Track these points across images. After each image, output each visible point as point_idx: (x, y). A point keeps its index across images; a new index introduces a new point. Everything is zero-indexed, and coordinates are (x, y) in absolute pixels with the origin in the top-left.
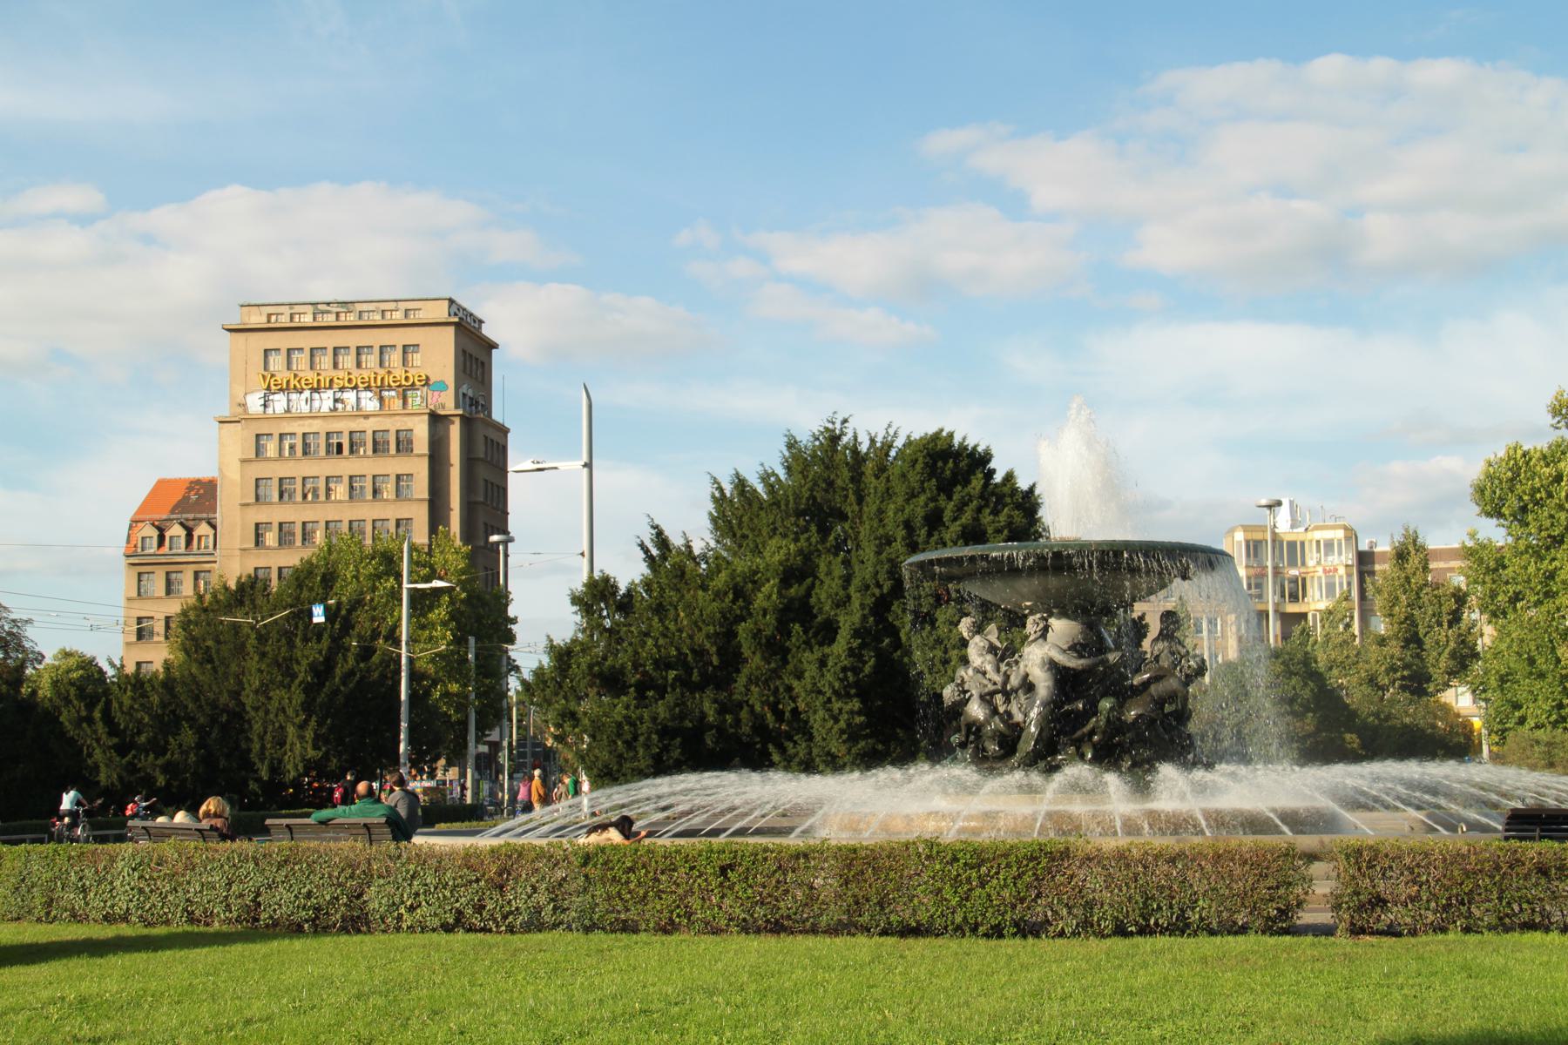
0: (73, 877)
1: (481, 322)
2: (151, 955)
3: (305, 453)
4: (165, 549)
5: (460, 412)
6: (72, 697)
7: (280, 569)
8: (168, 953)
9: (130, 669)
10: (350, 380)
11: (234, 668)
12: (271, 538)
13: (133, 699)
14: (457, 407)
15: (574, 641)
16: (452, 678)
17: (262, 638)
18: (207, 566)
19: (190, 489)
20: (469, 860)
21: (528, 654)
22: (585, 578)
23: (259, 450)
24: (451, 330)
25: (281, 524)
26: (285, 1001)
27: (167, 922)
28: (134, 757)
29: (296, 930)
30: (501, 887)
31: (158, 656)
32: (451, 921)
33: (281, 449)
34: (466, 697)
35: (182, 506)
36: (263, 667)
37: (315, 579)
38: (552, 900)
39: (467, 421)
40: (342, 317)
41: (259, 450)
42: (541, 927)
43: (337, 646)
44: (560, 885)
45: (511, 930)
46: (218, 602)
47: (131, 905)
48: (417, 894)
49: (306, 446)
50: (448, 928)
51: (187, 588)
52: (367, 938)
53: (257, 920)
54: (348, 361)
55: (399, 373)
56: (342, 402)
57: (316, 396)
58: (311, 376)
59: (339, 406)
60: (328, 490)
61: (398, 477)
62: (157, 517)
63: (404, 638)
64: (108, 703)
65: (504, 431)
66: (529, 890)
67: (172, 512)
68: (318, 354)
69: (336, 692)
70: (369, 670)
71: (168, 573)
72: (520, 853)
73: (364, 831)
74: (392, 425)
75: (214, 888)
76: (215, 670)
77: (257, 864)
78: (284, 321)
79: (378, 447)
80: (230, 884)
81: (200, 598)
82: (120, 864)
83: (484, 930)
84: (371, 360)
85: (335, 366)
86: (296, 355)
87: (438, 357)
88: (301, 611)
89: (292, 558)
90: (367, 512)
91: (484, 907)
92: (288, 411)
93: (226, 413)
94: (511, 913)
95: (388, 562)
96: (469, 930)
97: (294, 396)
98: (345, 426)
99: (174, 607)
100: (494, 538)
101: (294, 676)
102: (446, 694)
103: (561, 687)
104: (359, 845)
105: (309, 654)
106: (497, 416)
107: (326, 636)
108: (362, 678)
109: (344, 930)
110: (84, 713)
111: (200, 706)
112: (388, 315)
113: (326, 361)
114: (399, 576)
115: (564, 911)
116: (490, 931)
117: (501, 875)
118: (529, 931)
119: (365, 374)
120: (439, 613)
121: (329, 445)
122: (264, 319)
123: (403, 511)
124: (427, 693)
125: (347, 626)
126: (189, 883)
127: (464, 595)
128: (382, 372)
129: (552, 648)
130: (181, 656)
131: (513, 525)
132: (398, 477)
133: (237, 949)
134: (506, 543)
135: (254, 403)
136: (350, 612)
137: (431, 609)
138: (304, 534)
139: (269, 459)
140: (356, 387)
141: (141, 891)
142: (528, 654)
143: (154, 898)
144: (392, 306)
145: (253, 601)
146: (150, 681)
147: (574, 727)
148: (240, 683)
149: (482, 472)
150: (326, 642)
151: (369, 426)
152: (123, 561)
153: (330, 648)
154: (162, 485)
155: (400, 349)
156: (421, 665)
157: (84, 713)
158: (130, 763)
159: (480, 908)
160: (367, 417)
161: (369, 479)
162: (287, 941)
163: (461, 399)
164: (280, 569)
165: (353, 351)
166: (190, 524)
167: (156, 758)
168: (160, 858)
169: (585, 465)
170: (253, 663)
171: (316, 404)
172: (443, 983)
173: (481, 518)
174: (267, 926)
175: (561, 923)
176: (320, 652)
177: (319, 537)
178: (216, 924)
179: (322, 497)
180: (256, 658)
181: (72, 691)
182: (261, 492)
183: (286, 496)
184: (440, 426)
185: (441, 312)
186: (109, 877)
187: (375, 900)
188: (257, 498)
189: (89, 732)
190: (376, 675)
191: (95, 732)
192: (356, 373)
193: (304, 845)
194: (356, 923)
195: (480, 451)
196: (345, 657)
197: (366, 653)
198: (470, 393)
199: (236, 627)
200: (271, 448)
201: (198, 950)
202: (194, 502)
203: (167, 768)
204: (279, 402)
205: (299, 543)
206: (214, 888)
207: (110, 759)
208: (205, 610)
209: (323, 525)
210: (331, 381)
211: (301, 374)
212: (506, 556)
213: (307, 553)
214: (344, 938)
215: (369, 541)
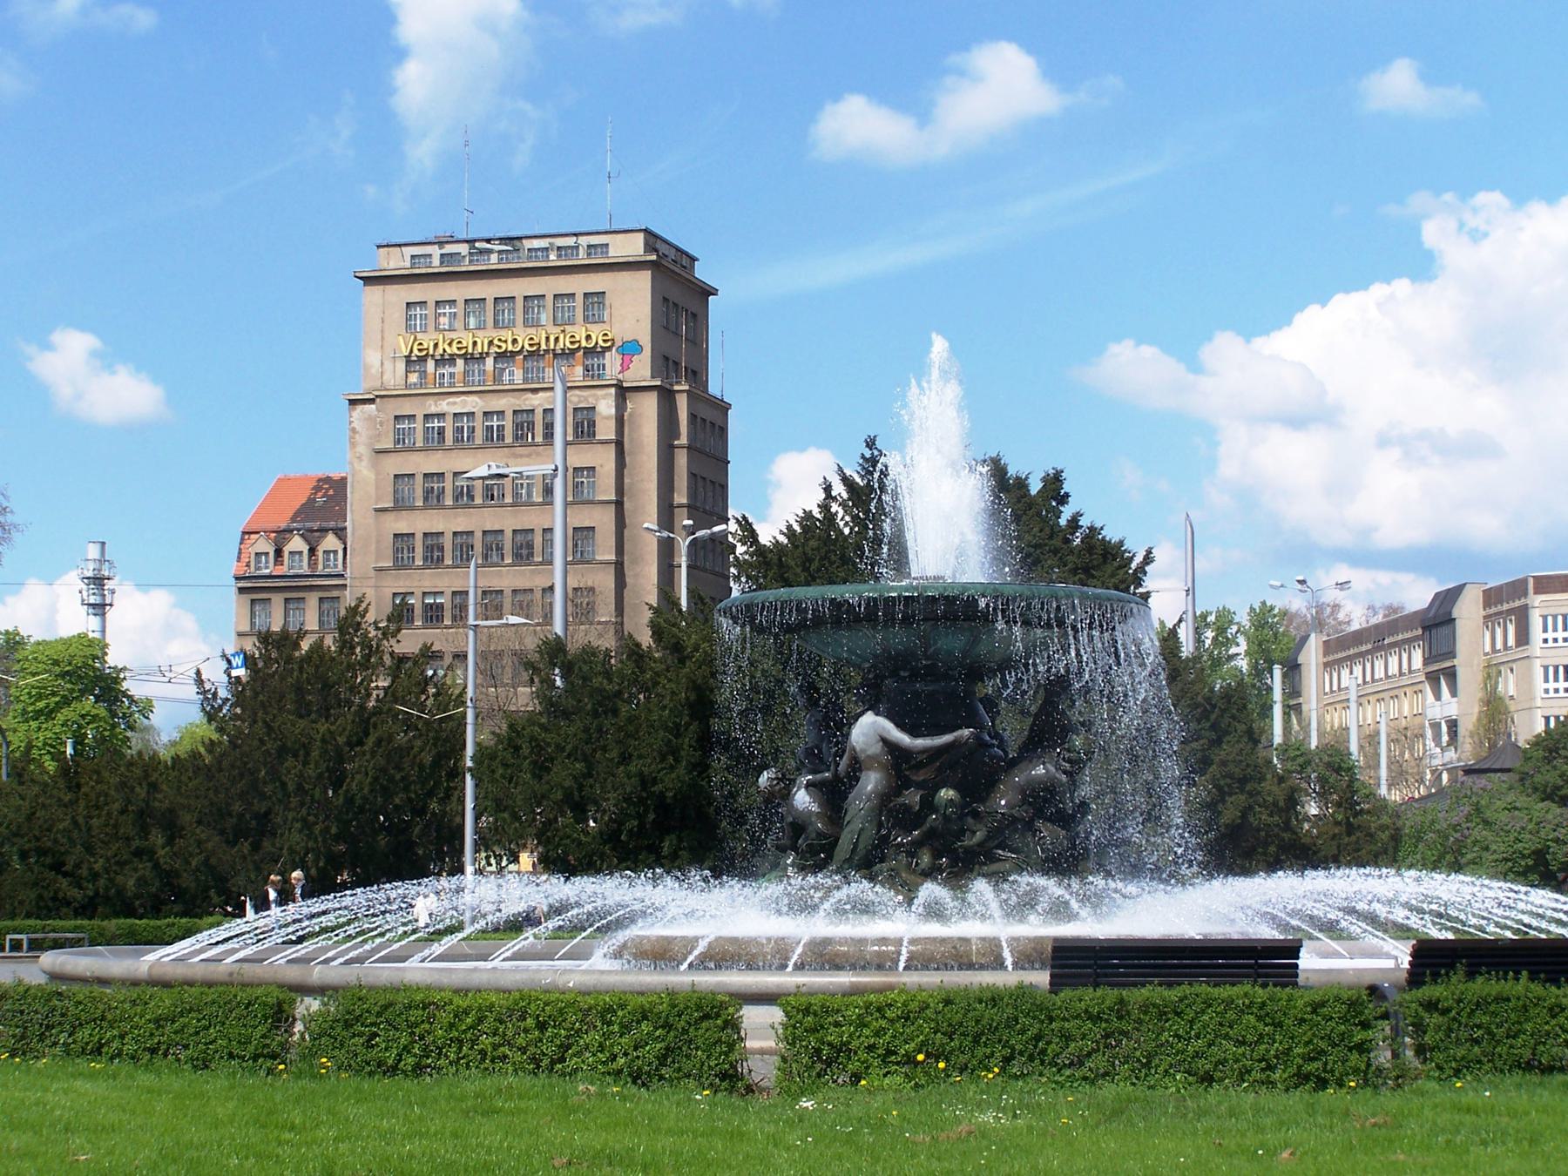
1: (694, 259)
14: (653, 377)
18: (335, 593)
19: (317, 489)
67: (293, 520)
87: (631, 307)
122: (408, 264)
144: (570, 241)
185: (633, 247)
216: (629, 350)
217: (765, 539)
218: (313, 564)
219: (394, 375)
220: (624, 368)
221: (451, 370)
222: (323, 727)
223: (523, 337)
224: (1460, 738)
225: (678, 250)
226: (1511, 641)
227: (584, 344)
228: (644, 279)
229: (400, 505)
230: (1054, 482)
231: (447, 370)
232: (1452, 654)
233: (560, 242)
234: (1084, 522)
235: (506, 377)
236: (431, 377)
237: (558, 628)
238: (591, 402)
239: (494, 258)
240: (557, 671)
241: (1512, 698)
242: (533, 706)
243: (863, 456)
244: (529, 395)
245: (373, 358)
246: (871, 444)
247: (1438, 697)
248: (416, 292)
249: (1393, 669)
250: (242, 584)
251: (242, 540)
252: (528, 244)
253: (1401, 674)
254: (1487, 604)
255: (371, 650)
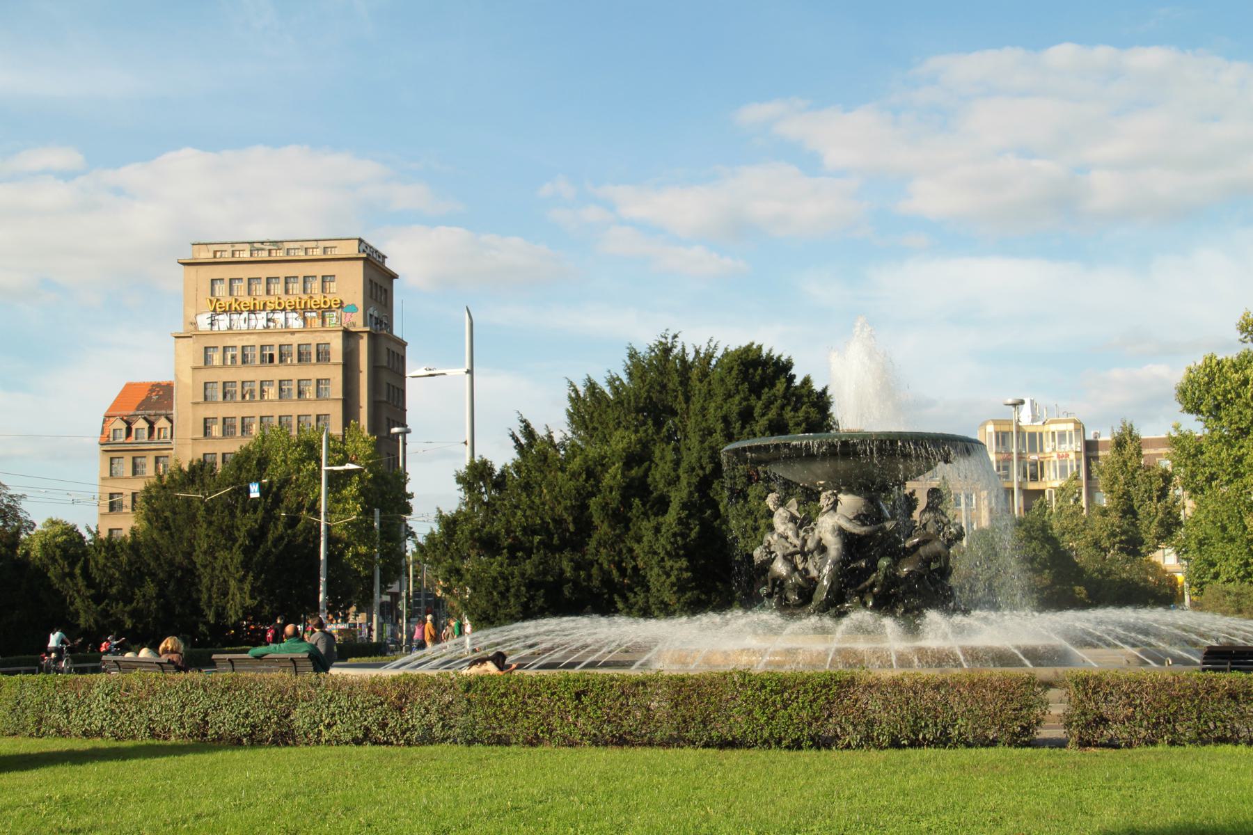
0: (58, 701)
1: (384, 257)
2: (121, 763)
3: (244, 362)
4: (132, 439)
5: (368, 329)
6: (57, 557)
7: (224, 455)
8: (134, 761)
9: (104, 534)
10: (280, 304)
11: (187, 534)
12: (216, 430)
13: (106, 558)
14: (365, 325)
15: (459, 512)
16: (361, 542)
17: (209, 510)
18: (165, 453)
19: (152, 391)
20: (375, 687)
21: (422, 523)
22: (467, 462)
23: (207, 360)
24: (361, 263)
25: (224, 419)
26: (227, 800)
27: (134, 737)
28: (107, 605)
29: (237, 743)
30: (401, 709)
31: (126, 524)
32: (360, 736)
33: (224, 359)
34: (373, 557)
35: (145, 404)
36: (211, 533)
37: (252, 463)
38: (441, 719)
39: (373, 337)
40: (274, 253)
41: (207, 360)
42: (432, 741)
43: (270, 516)
44: (448, 707)
45: (408, 743)
46: (174, 481)
47: (105, 723)
48: (333, 715)
49: (244, 356)
50: (358, 742)
51: (149, 470)
52: (293, 750)
53: (206, 735)
54: (278, 288)
55: (319, 298)
56: (274, 321)
57: (253, 316)
58: (249, 301)
59: (271, 324)
60: (262, 391)
61: (318, 381)
62: (125, 413)
63: (323, 510)
64: (87, 562)
65: (403, 344)
66: (423, 711)
67: (138, 409)
68: (254, 283)
69: (268, 553)
70: (295, 536)
71: (134, 458)
72: (416, 681)
73: (291, 664)
74: (313, 339)
75: (171, 709)
76: (172, 535)
77: (205, 691)
78: (227, 256)
79: (302, 357)
80: (183, 707)
81: (160, 478)
82: (96, 691)
83: (387, 743)
84: (296, 288)
85: (268, 292)
86: (236, 284)
87: (350, 285)
88: (241, 488)
89: (233, 446)
90: (293, 409)
91: (387, 725)
92: (230, 328)
93: (180, 330)
94: (408, 729)
95: (310, 449)
96: (375, 743)
97: (235, 317)
98: (275, 340)
99: (139, 485)
100: (395, 430)
101: (235, 540)
102: (357, 555)
103: (448, 549)
104: (287, 675)
105: (247, 522)
106: (397, 332)
107: (260, 508)
108: (290, 542)
109: (275, 743)
110: (67, 570)
111: (160, 564)
112: (310, 251)
113: (260, 289)
114: (318, 460)
115: (451, 728)
116: (392, 744)
117: (400, 699)
118: (423, 744)
119: (292, 299)
120: (351, 490)
121: (263, 356)
122: (211, 255)
123: (322, 408)
124: (342, 554)
125: (278, 500)
126: (151, 705)
127: (370, 476)
128: (305, 297)
129: (441, 518)
130: (145, 524)
131: (410, 419)
132: (318, 381)
133: (190, 758)
134: (404, 434)
135: (203, 322)
136: (279, 489)
137: (344, 486)
138: (243, 427)
139: (215, 367)
140: (284, 309)
141: (113, 712)
142: (422, 523)
143: (123, 718)
144: (313, 244)
145: (202, 480)
146: (120, 544)
147: (459, 581)
148: (192, 546)
149: (386, 377)
150: (260, 513)
151: (295, 340)
152: (99, 449)
153: (263, 518)
154: (129, 388)
155: (319, 279)
156: (336, 531)
157: (67, 570)
158: (104, 610)
159: (383, 726)
160: (293, 333)
161: (295, 382)
162: (229, 752)
163: (368, 319)
164: (224, 455)
165: (282, 281)
166: (152, 418)
167: (125, 606)
168: (128, 686)
169: (468, 372)
170: (202, 530)
171: (253, 323)
172: (354, 785)
173: (385, 414)
174: (214, 740)
175: (448, 737)
176: (256, 521)
177: (255, 429)
178: (173, 738)
179: (258, 398)
180: (205, 526)
181: (58, 552)
182: (209, 393)
183: (229, 396)
184: (352, 341)
185: (352, 249)
186: (87, 701)
187: (300, 719)
188: (206, 398)
189: (71, 585)
190: (300, 539)
191: (76, 585)
192: (284, 298)
193: (243, 675)
194: (285, 738)
195: (384, 360)
196: (276, 525)
197: (293, 521)
198: (376, 314)
199: (188, 501)
200: (217, 358)
201: (158, 759)
202: (155, 401)
203: (134, 614)
204: (223, 322)
205: (239, 434)
206: (171, 709)
207: (88, 607)
208: (164, 488)
209: (258, 419)
210: (265, 304)
211: (240, 299)
212: (405, 444)
213: (245, 442)
214: (275, 750)
215: (295, 433)
228: (360, 265)
238: (327, 340)
248: (217, 272)
250: (106, 448)
251: (104, 421)
252: (287, 245)
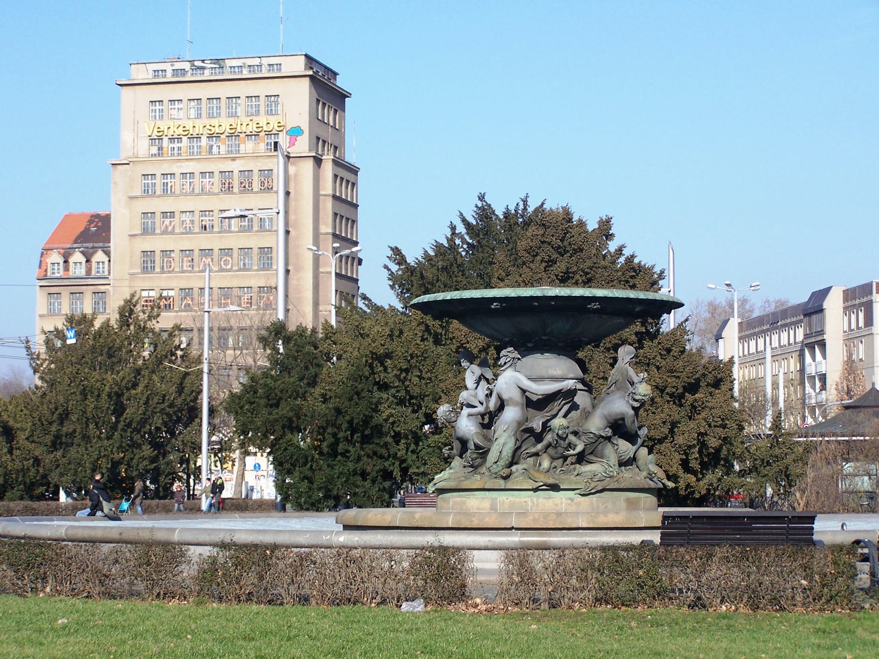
1: (335, 74)
14: (310, 150)
19: (91, 222)
122: (151, 76)
185: (298, 65)
216: (294, 133)
217: (411, 260)
218: (67, 269)
219: (144, 148)
220: (292, 144)
221: (179, 145)
222: (109, 377)
223: (224, 124)
224: (828, 386)
225: (326, 68)
226: (861, 324)
227: (265, 128)
229: (147, 231)
230: (605, 226)
231: (176, 145)
232: (822, 332)
233: (250, 62)
234: (627, 252)
235: (215, 150)
236: (165, 150)
237: (281, 316)
239: (207, 72)
240: (280, 342)
241: (861, 360)
242: (264, 363)
243: (477, 206)
244: (230, 162)
245: (127, 137)
246: (481, 198)
247: (814, 359)
249: (784, 341)
251: (42, 254)
252: (229, 63)
253: (789, 344)
254: (846, 299)
255: (143, 329)
